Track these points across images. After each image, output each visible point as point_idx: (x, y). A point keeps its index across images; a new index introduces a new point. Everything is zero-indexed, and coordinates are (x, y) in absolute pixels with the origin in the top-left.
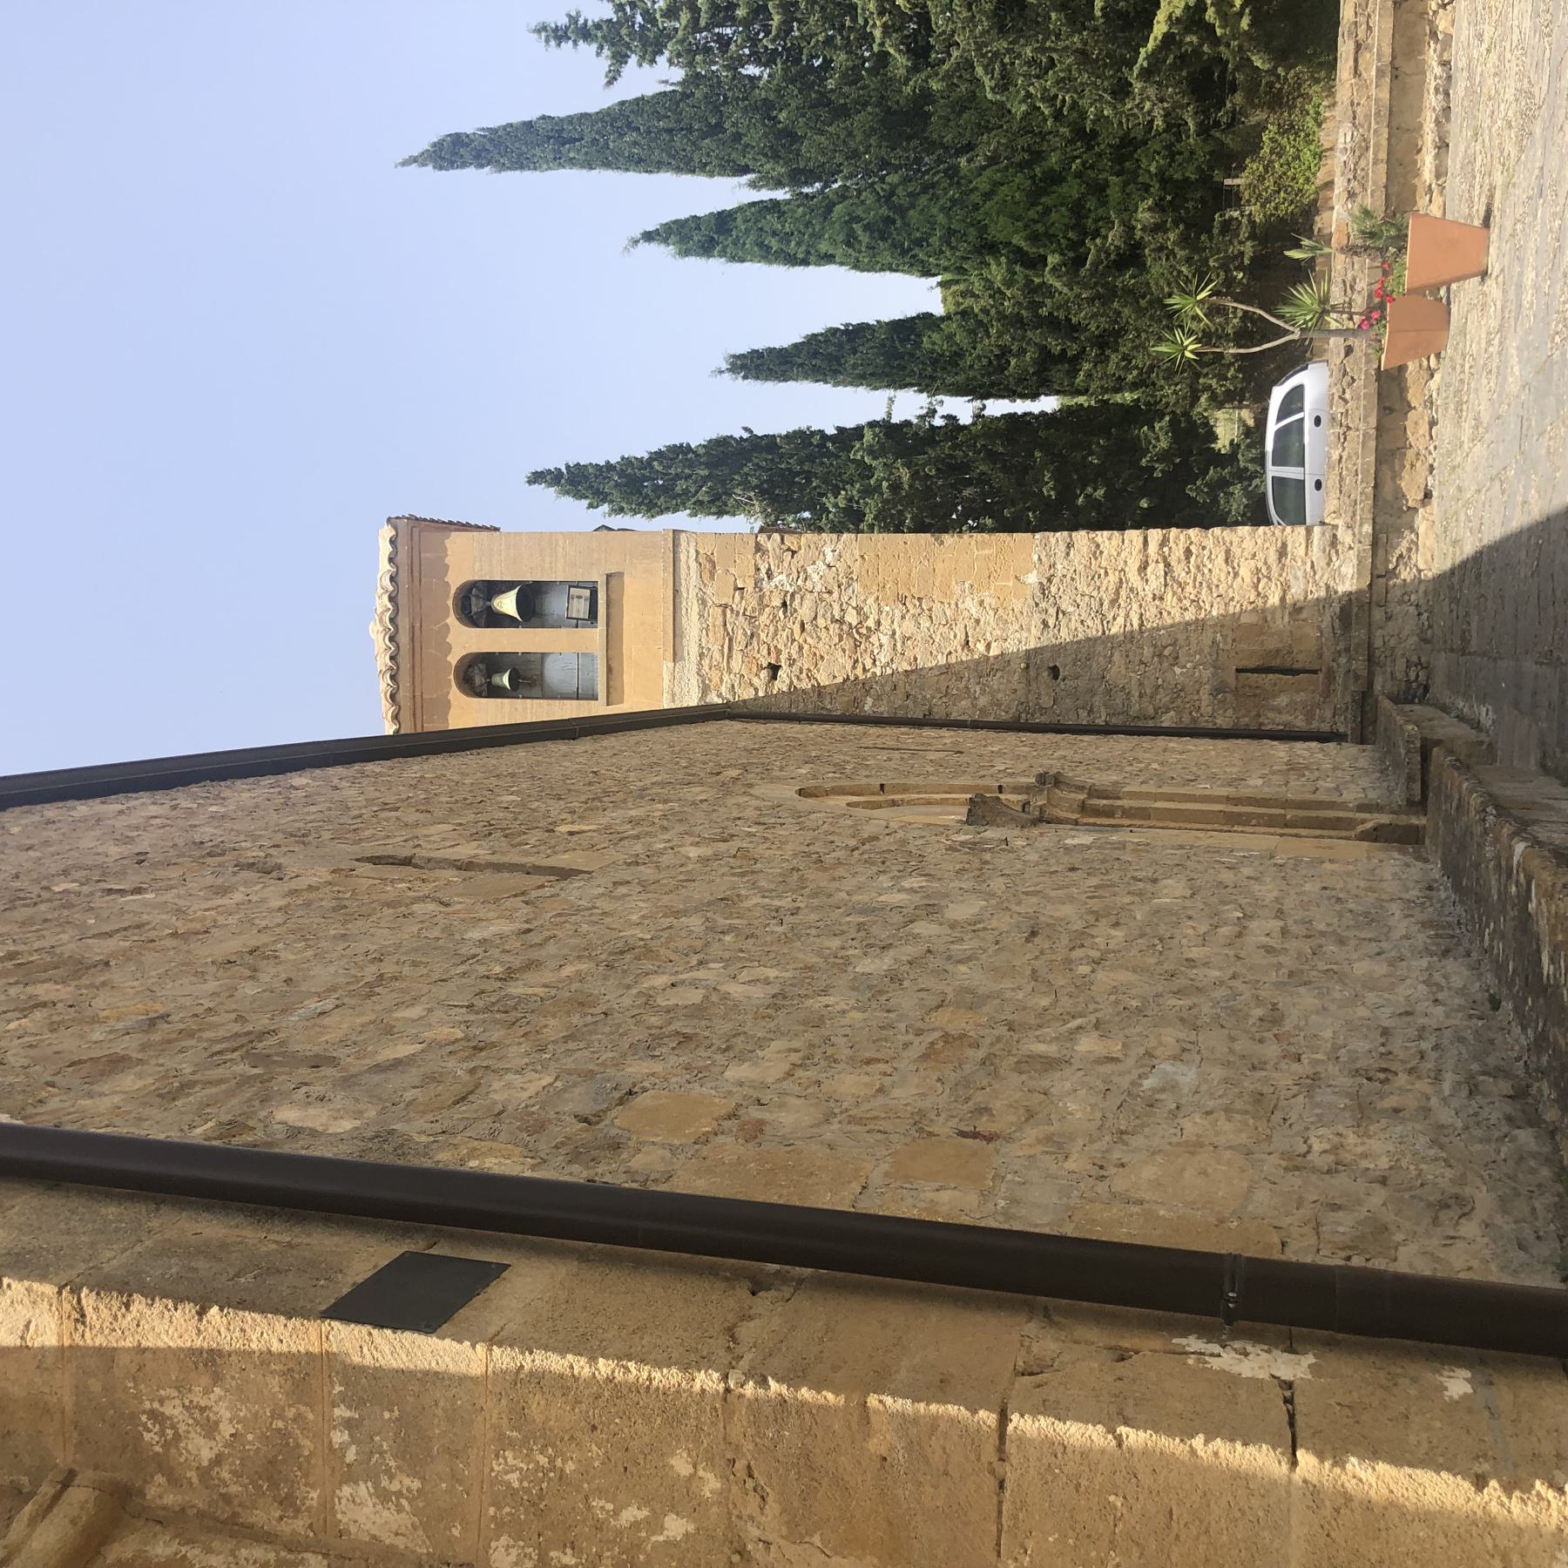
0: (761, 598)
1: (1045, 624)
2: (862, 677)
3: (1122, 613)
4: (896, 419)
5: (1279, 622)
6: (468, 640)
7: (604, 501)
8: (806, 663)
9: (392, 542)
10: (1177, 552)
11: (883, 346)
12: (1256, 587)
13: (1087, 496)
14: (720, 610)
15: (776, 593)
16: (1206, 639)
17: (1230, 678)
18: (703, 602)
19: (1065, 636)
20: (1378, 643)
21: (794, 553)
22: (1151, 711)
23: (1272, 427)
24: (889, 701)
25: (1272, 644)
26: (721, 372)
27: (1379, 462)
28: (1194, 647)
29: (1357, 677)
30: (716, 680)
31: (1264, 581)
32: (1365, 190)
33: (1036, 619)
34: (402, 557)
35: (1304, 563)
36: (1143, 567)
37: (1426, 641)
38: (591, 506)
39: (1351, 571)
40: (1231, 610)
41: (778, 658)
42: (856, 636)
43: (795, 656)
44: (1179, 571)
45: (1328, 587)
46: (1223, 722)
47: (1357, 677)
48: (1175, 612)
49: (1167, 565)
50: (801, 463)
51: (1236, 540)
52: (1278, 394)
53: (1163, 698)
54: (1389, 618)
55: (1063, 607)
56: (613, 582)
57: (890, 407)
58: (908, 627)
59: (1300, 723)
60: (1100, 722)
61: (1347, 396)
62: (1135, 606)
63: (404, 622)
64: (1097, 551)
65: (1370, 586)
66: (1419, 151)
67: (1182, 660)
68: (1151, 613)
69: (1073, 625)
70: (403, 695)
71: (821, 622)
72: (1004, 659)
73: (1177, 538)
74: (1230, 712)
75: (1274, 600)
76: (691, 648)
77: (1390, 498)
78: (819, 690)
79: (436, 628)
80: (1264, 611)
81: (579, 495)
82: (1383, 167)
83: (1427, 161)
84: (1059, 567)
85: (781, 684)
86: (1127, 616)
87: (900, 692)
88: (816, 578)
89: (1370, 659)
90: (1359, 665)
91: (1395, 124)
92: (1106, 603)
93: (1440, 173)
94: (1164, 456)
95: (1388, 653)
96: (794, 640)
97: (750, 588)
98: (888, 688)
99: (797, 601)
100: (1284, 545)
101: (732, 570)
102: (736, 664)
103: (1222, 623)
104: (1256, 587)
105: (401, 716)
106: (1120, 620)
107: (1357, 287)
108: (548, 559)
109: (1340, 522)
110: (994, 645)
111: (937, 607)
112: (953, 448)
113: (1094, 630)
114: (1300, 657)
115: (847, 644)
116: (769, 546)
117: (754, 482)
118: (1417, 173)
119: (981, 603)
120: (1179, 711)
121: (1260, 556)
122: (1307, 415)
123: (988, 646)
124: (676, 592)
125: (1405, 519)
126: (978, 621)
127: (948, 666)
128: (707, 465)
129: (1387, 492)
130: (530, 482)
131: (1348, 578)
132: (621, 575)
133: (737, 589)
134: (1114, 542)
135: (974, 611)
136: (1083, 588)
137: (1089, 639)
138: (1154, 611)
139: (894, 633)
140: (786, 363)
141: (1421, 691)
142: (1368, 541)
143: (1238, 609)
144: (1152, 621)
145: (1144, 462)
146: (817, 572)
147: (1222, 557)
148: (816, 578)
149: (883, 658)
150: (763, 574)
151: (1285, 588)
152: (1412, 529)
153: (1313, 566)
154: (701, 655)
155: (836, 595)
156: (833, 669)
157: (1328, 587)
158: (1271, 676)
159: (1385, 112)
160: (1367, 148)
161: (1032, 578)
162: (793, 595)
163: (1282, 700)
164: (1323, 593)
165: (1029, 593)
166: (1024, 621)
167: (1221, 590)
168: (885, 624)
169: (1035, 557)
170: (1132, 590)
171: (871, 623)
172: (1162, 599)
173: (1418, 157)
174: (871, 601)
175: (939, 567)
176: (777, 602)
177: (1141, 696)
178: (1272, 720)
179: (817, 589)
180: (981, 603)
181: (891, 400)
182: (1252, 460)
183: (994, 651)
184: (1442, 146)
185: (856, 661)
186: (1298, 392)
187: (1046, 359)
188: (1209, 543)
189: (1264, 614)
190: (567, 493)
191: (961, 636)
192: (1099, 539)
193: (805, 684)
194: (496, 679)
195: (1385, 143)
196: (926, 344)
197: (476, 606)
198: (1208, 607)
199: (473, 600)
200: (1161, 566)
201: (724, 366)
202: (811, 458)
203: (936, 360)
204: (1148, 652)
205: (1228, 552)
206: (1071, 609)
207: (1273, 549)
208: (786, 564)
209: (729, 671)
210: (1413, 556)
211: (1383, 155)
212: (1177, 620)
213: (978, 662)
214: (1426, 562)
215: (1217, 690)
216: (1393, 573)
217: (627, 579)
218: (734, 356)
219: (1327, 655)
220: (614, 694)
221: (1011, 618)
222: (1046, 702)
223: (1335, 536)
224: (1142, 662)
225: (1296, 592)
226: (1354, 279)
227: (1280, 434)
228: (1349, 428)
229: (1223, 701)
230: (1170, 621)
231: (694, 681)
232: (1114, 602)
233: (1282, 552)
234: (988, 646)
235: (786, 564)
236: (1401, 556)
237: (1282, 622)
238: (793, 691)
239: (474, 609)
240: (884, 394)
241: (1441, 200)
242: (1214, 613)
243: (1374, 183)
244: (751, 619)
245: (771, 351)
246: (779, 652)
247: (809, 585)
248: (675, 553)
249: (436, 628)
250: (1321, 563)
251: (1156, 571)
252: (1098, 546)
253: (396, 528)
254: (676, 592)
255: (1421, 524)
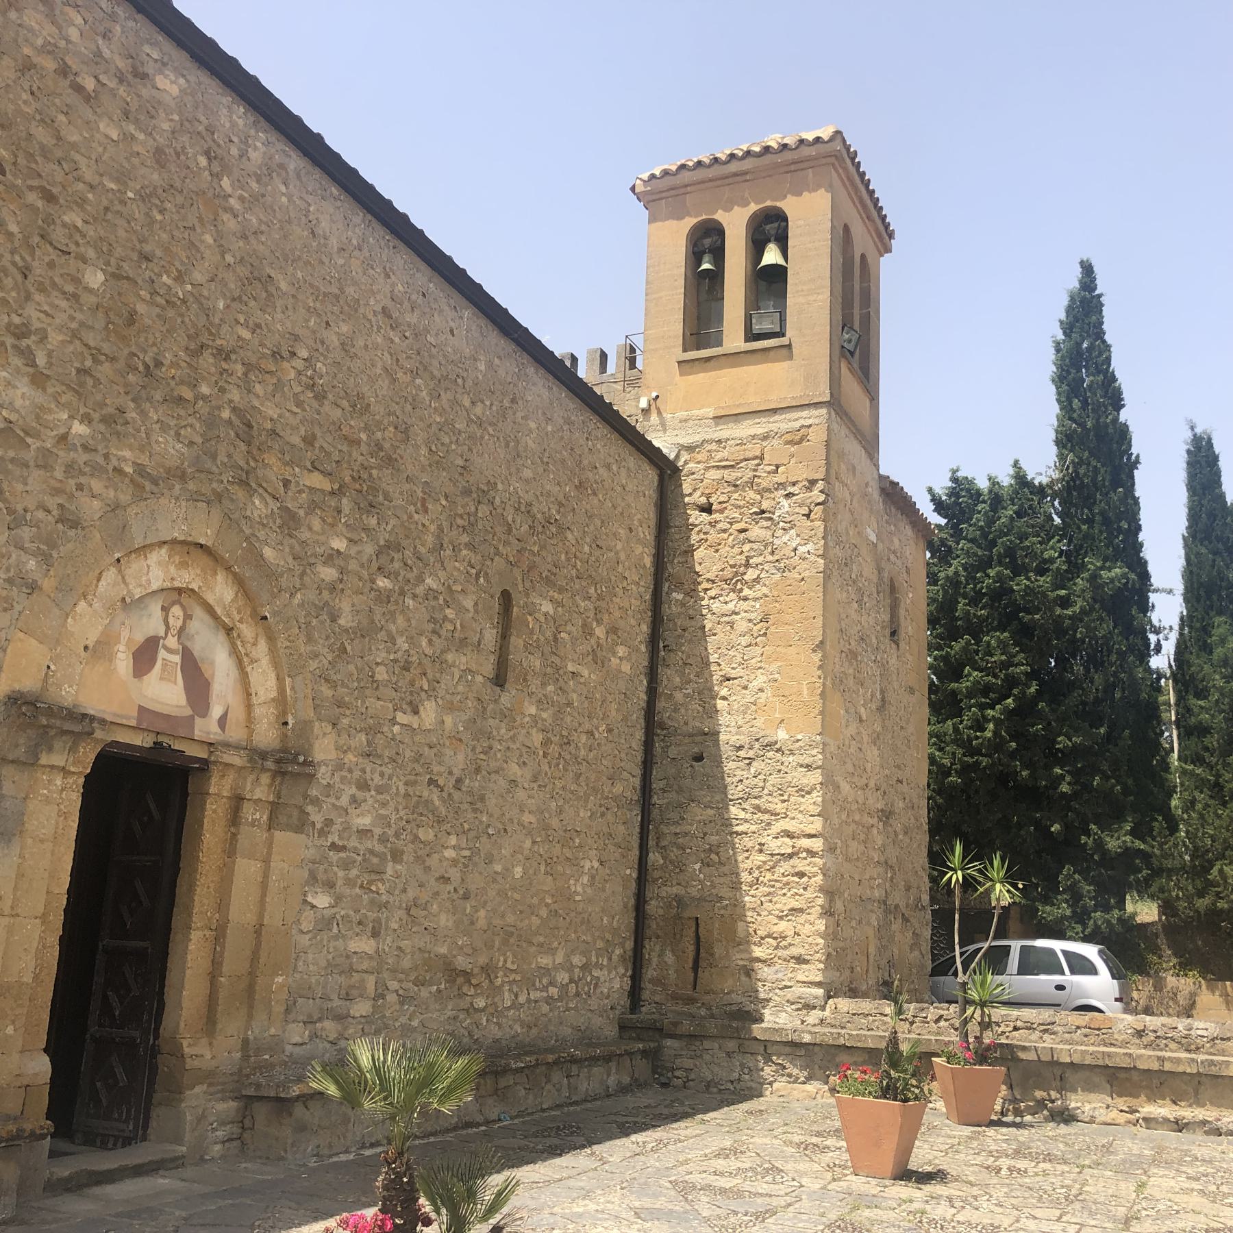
0: (769, 490)
1: (740, 748)
2: (700, 588)
3: (748, 816)
4: (1153, 597)
5: (738, 956)
6: (736, 225)
7: (1065, 333)
8: (713, 536)
9: (818, 139)
10: (800, 864)
11: (1222, 580)
12: (769, 936)
13: (1062, 777)
14: (758, 453)
15: (773, 503)
16: (724, 892)
17: (689, 913)
18: (766, 438)
19: (729, 766)
20: (707, 1044)
21: (808, 516)
22: (663, 844)
23: (1057, 945)
24: (680, 614)
25: (718, 951)
26: (1192, 428)
27: (870, 1051)
28: (717, 880)
29: (675, 1024)
30: (699, 457)
31: (774, 943)
32: (1145, 1047)
33: (743, 740)
34: (806, 151)
35: (790, 980)
36: (789, 835)
37: (708, 1086)
38: (1061, 322)
39: (781, 1021)
40: (749, 914)
41: (717, 511)
42: (734, 581)
43: (718, 526)
44: (785, 867)
45: (768, 1000)
46: (653, 907)
47: (675, 1024)
48: (748, 863)
49: (790, 856)
50: (1102, 513)
51: (811, 918)
52: (1090, 951)
53: (674, 853)
54: (728, 1054)
55: (755, 764)
56: (785, 352)
57: (1163, 591)
58: (742, 626)
59: (650, 973)
60: (655, 799)
61: (942, 1023)
62: (753, 828)
63: (748, 164)
64: (803, 792)
65: (756, 1039)
66: (1175, 1103)
67: (707, 870)
68: (747, 842)
69: (738, 772)
70: (686, 176)
71: (746, 547)
72: (712, 713)
73: (815, 865)
74: (661, 912)
75: (758, 952)
76: (726, 431)
77: (837, 1060)
78: (690, 551)
79: (747, 195)
80: (748, 942)
81: (1069, 310)
82: (1155, 1066)
83: (1163, 1110)
84: (791, 758)
85: (696, 517)
86: (746, 821)
87: (688, 623)
88: (785, 539)
89: (692, 1037)
90: (686, 1027)
91: (1203, 1079)
92: (756, 802)
93: (1149, 1121)
94: (1100, 844)
95: (699, 1053)
96: (731, 524)
97: (779, 478)
98: (691, 612)
99: (765, 523)
100: (806, 962)
101: (793, 461)
102: (714, 474)
103: (737, 905)
104: (769, 936)
105: (668, 178)
106: (742, 815)
107: (1046, 1036)
108: (805, 288)
109: (827, 1013)
110: (726, 703)
111: (759, 650)
112: (1119, 652)
113: (734, 792)
114: (707, 973)
115: (728, 573)
116: (816, 492)
117: (1082, 471)
118: (1151, 1099)
119: (761, 690)
120: (662, 867)
121: (797, 940)
122: (1068, 978)
123: (724, 698)
124: (775, 411)
125: (819, 1073)
126: (745, 688)
127: (708, 664)
128: (1097, 426)
129: (844, 1058)
130: (1082, 263)
131: (777, 1019)
132: (791, 357)
133: (777, 467)
134: (811, 808)
135: (755, 684)
136: (772, 780)
137: (726, 787)
138: (750, 844)
139: (737, 614)
140: (1204, 489)
141: (663, 1080)
142: (796, 1038)
143: (749, 919)
144: (742, 843)
145: (1093, 826)
146: (787, 540)
147: (797, 905)
148: (785, 539)
149: (716, 606)
150: (790, 489)
151: (768, 962)
152: (809, 1079)
153: (786, 987)
154: (719, 441)
155: (770, 558)
156: (707, 562)
157: (768, 1000)
158: (692, 948)
159: (1214, 1070)
160: (1189, 1051)
161: (782, 735)
162: (770, 519)
163: (670, 958)
164: (762, 996)
165: (768, 732)
166: (745, 729)
167: (766, 905)
168: (744, 605)
169: (799, 737)
170: (769, 824)
171: (746, 592)
172: (761, 851)
173: (1168, 1101)
174: (765, 590)
175: (793, 650)
176: (765, 506)
177: (676, 834)
178: (652, 950)
179: (776, 541)
180: (761, 690)
181: (1170, 592)
182: (1097, 927)
183: (720, 704)
184: (1179, 1126)
185: (713, 582)
186: (1091, 970)
187: (1203, 731)
188: (810, 894)
189: (743, 943)
190: (1072, 299)
191: (733, 674)
192: (815, 794)
193: (694, 538)
194: (706, 257)
195: (1180, 1069)
196: (1218, 620)
197: (771, 228)
198: (752, 892)
199: (776, 225)
200: (790, 851)
201: (1198, 430)
202: (1106, 521)
203: (1206, 630)
204: (714, 839)
205: (801, 911)
206: (753, 770)
207: (802, 951)
208: (797, 510)
209: (707, 469)
210: (784, 1079)
211: (1168, 1066)
212: (741, 865)
213: (711, 689)
214: (778, 1090)
215: (680, 900)
216: (768, 1060)
217: (786, 364)
218: (1210, 439)
219: (707, 998)
220: (687, 366)
221: (748, 717)
222: (673, 752)
223: (814, 1008)
224: (705, 834)
225: (765, 972)
226: (1054, 1033)
227: (1052, 952)
228: (912, 1023)
229: (670, 906)
230: (740, 858)
231: (698, 438)
232: (758, 808)
233: (800, 960)
234: (724, 698)
235: (797, 510)
236: (784, 1068)
237: (738, 959)
238: (689, 528)
239: (768, 227)
240: (1179, 586)
241: (1122, 1121)
242: (747, 899)
243: (1140, 1056)
244: (751, 483)
245: (1218, 474)
246: (721, 511)
247: (779, 533)
248: (809, 405)
249: (747, 195)
250: (789, 994)
251: (785, 845)
252: (809, 793)
253: (832, 139)
254: (775, 411)
255: (812, 1087)
